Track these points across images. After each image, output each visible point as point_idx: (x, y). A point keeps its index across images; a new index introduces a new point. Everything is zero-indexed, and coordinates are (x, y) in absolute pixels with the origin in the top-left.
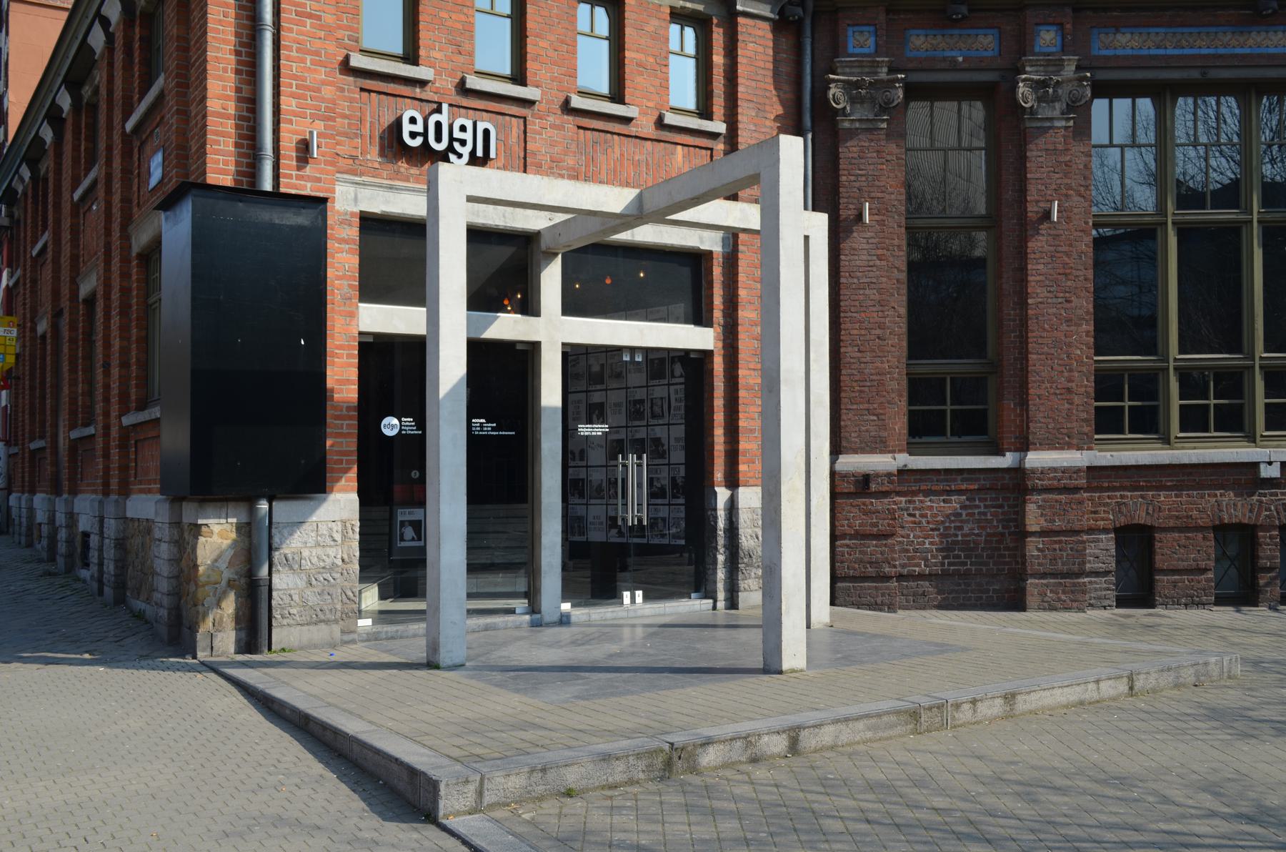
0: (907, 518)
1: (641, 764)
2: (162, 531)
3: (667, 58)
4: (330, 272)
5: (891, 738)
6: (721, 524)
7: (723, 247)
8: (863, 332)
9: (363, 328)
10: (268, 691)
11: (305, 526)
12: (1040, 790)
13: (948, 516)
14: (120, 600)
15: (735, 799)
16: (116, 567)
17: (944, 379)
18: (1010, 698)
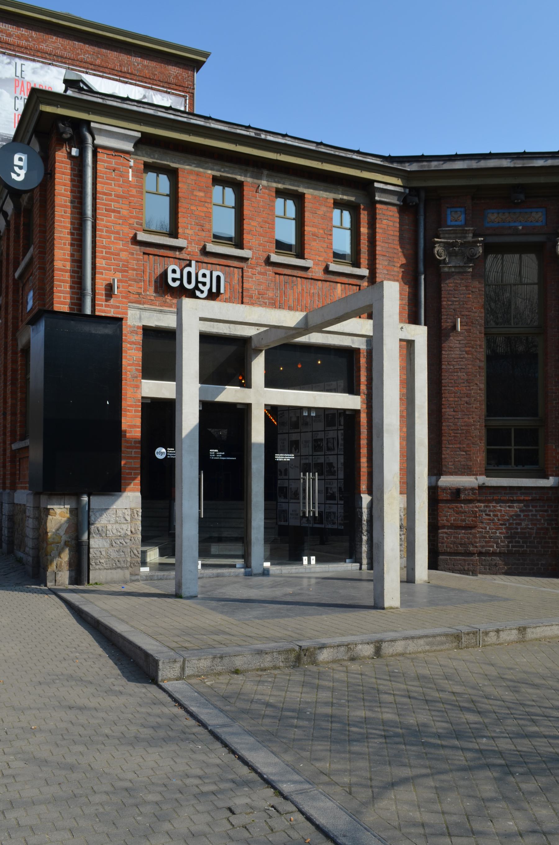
0: (485, 517)
1: (282, 658)
2: (30, 512)
3: (331, 230)
4: (124, 361)
5: (441, 650)
6: (365, 517)
7: (367, 346)
8: (456, 399)
9: (144, 395)
10: (80, 606)
11: (109, 511)
12: (523, 685)
13: (511, 516)
14: (11, 551)
15: (334, 680)
16: (9, 532)
17: (511, 429)
18: (522, 630)
